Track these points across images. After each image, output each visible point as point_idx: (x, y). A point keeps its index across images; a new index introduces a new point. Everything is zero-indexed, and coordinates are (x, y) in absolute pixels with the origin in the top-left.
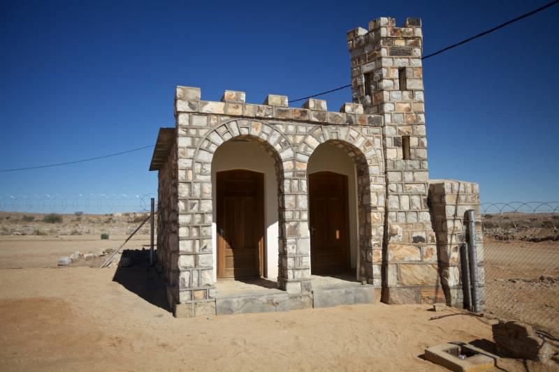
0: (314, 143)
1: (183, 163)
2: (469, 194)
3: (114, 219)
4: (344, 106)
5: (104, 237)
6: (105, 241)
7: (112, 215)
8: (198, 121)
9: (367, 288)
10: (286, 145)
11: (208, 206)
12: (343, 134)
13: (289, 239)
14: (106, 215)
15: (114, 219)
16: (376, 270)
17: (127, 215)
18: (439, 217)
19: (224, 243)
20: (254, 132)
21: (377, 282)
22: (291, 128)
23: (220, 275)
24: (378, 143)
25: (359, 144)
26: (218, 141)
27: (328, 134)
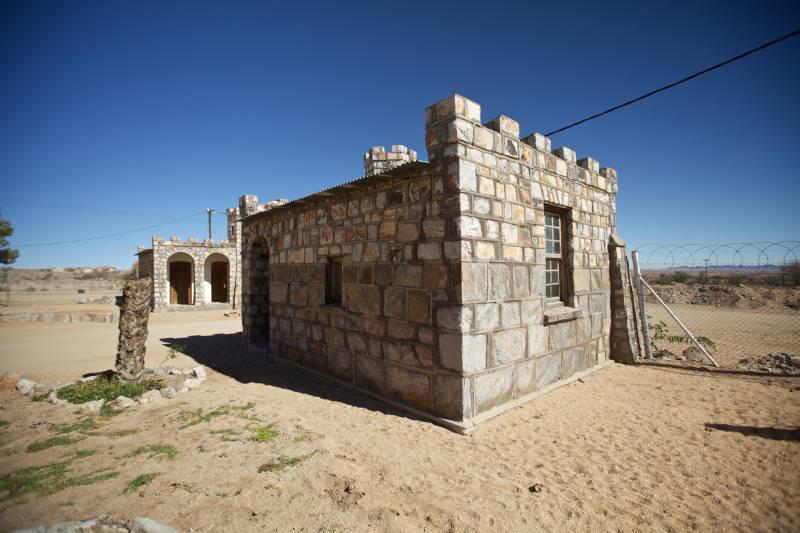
0: (207, 254)
1: (156, 262)
2: (650, 255)
3: (54, 275)
4: (498, 118)
5: (81, 291)
6: (80, 295)
7: (49, 270)
8: (161, 248)
9: (227, 304)
10: (196, 255)
11: (165, 277)
12: (219, 251)
13: (204, 289)
14: (42, 270)
15: (54, 275)
16: (231, 298)
17: (71, 270)
18: (616, 282)
19: (173, 290)
20: (184, 251)
21: (231, 302)
22: (198, 249)
23: (171, 302)
24: (234, 253)
25: (226, 254)
26: (169, 254)
27: (213, 251)
